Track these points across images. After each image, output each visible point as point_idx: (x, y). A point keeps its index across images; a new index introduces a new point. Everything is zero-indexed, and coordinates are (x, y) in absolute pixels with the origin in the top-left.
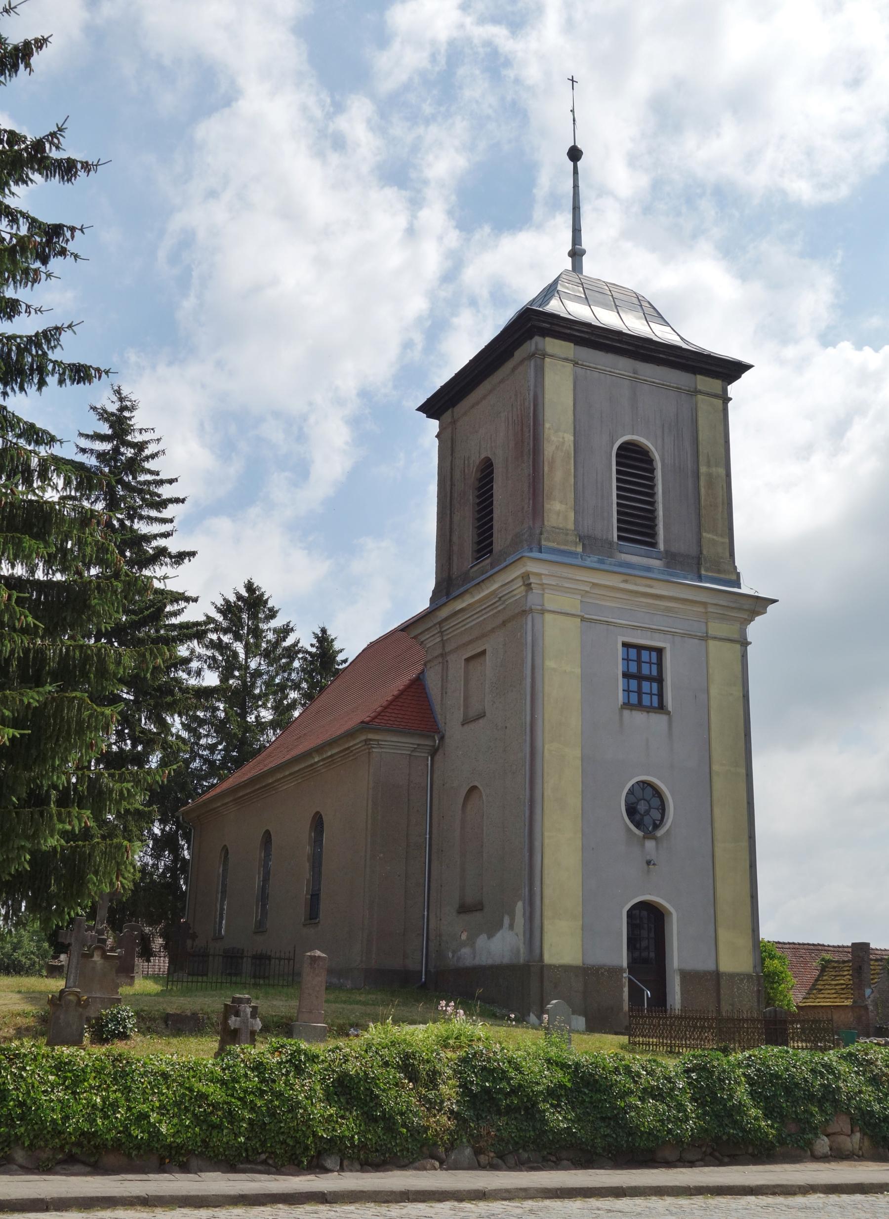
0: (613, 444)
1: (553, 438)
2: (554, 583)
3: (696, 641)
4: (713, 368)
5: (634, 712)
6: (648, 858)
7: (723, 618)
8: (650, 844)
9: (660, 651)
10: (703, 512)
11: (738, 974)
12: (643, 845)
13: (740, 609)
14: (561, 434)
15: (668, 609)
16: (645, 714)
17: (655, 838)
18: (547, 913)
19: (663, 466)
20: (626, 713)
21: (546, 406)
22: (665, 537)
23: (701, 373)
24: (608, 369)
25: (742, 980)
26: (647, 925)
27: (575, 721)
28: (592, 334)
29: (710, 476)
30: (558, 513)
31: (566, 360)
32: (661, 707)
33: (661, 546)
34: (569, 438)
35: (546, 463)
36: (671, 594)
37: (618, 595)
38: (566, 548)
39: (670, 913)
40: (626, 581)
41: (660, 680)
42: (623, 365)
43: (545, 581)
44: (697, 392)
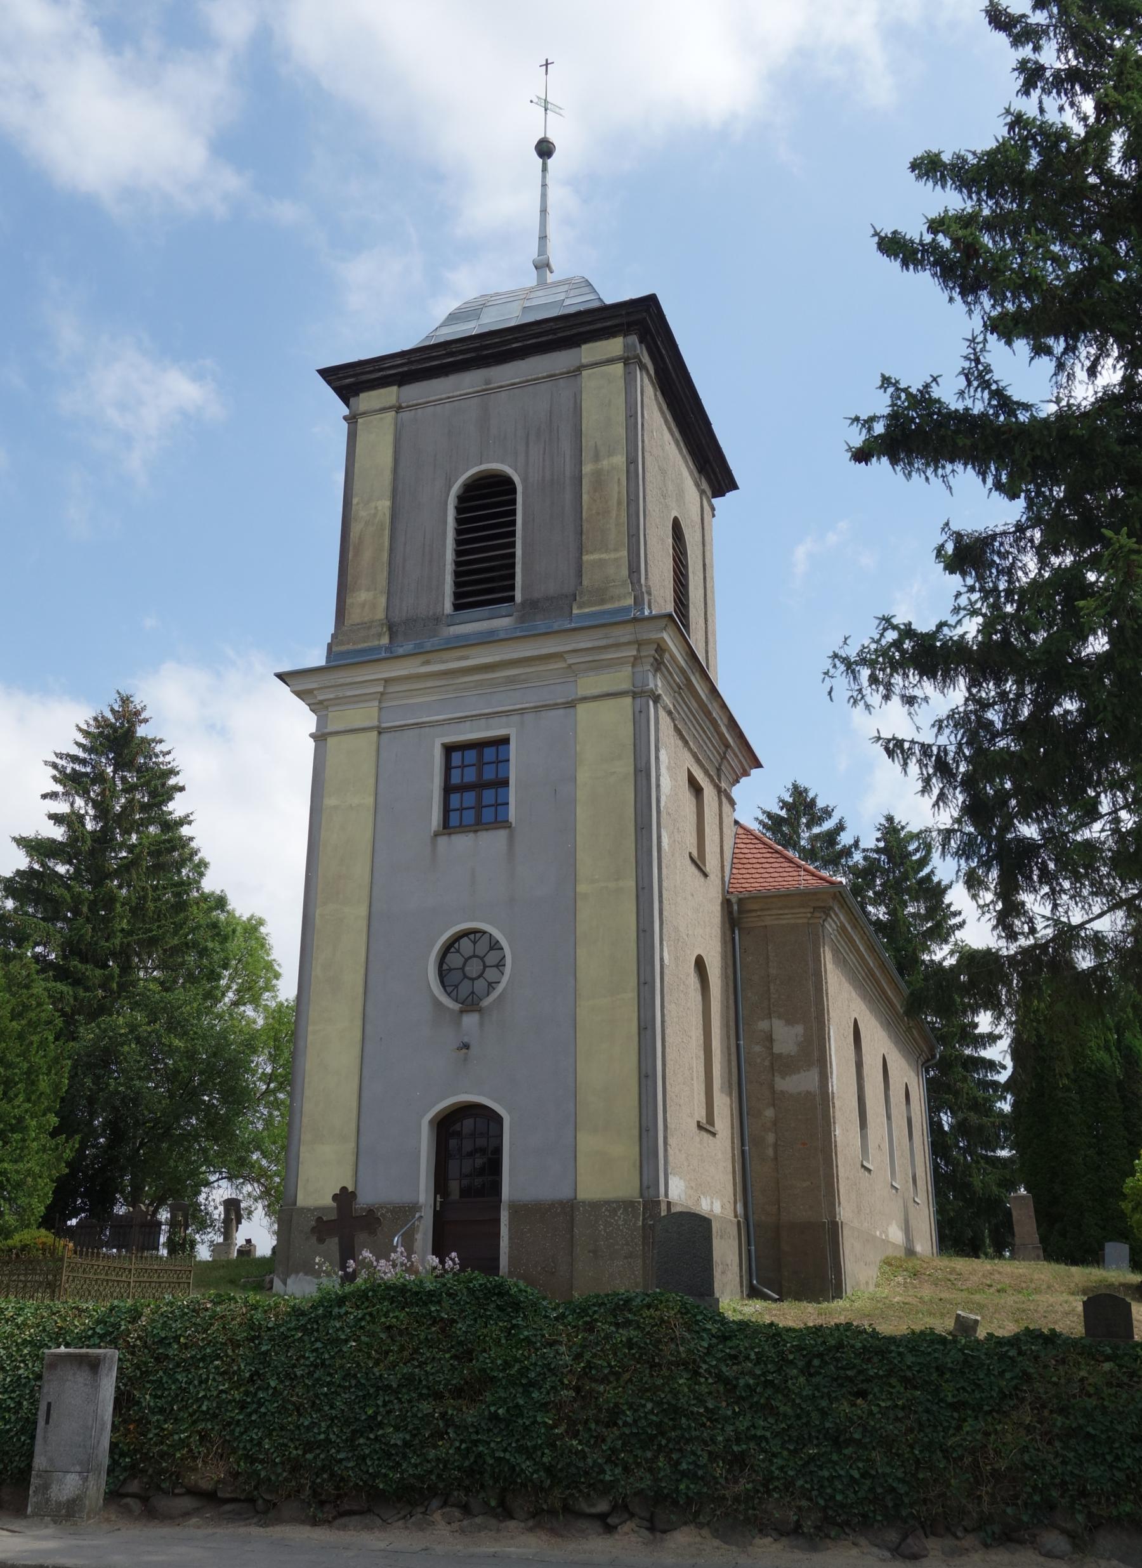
0: (450, 488)
1: (363, 513)
2: (332, 696)
3: (561, 712)
4: (599, 325)
5: (454, 837)
6: (466, 1040)
7: (599, 666)
8: (470, 1020)
9: (449, 749)
10: (585, 526)
11: (607, 1202)
12: (458, 1024)
13: (617, 646)
14: (373, 505)
15: (511, 680)
16: (471, 835)
17: (480, 1010)
18: (306, 1137)
19: (525, 488)
20: (443, 841)
21: (355, 477)
22: (523, 581)
23: (586, 341)
24: (444, 396)
25: (615, 1211)
26: (467, 1143)
27: (360, 870)
28: (410, 363)
29: (598, 474)
30: (363, 605)
31: (384, 410)
32: (505, 824)
33: (518, 597)
34: (385, 504)
35: (351, 548)
36: (497, 658)
37: (429, 684)
38: (366, 645)
39: (431, 1122)
40: (427, 663)
41: (448, 789)
42: (470, 381)
43: (320, 698)
44: (580, 368)
